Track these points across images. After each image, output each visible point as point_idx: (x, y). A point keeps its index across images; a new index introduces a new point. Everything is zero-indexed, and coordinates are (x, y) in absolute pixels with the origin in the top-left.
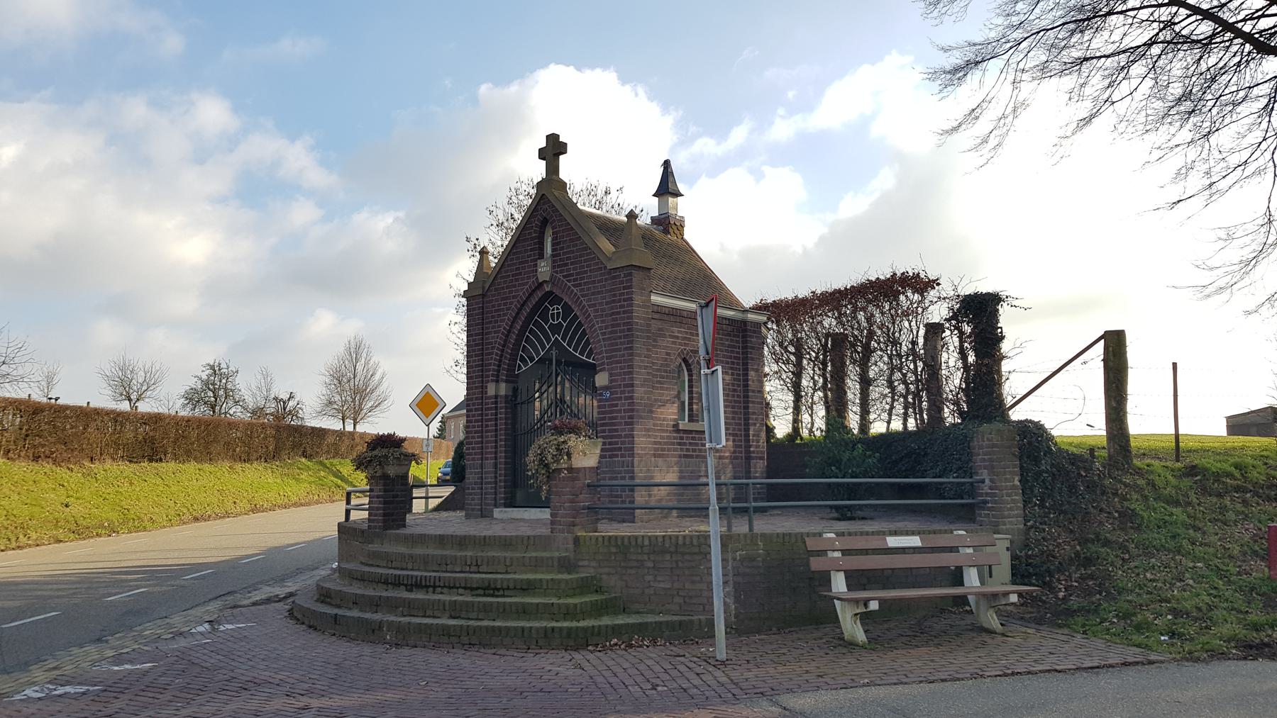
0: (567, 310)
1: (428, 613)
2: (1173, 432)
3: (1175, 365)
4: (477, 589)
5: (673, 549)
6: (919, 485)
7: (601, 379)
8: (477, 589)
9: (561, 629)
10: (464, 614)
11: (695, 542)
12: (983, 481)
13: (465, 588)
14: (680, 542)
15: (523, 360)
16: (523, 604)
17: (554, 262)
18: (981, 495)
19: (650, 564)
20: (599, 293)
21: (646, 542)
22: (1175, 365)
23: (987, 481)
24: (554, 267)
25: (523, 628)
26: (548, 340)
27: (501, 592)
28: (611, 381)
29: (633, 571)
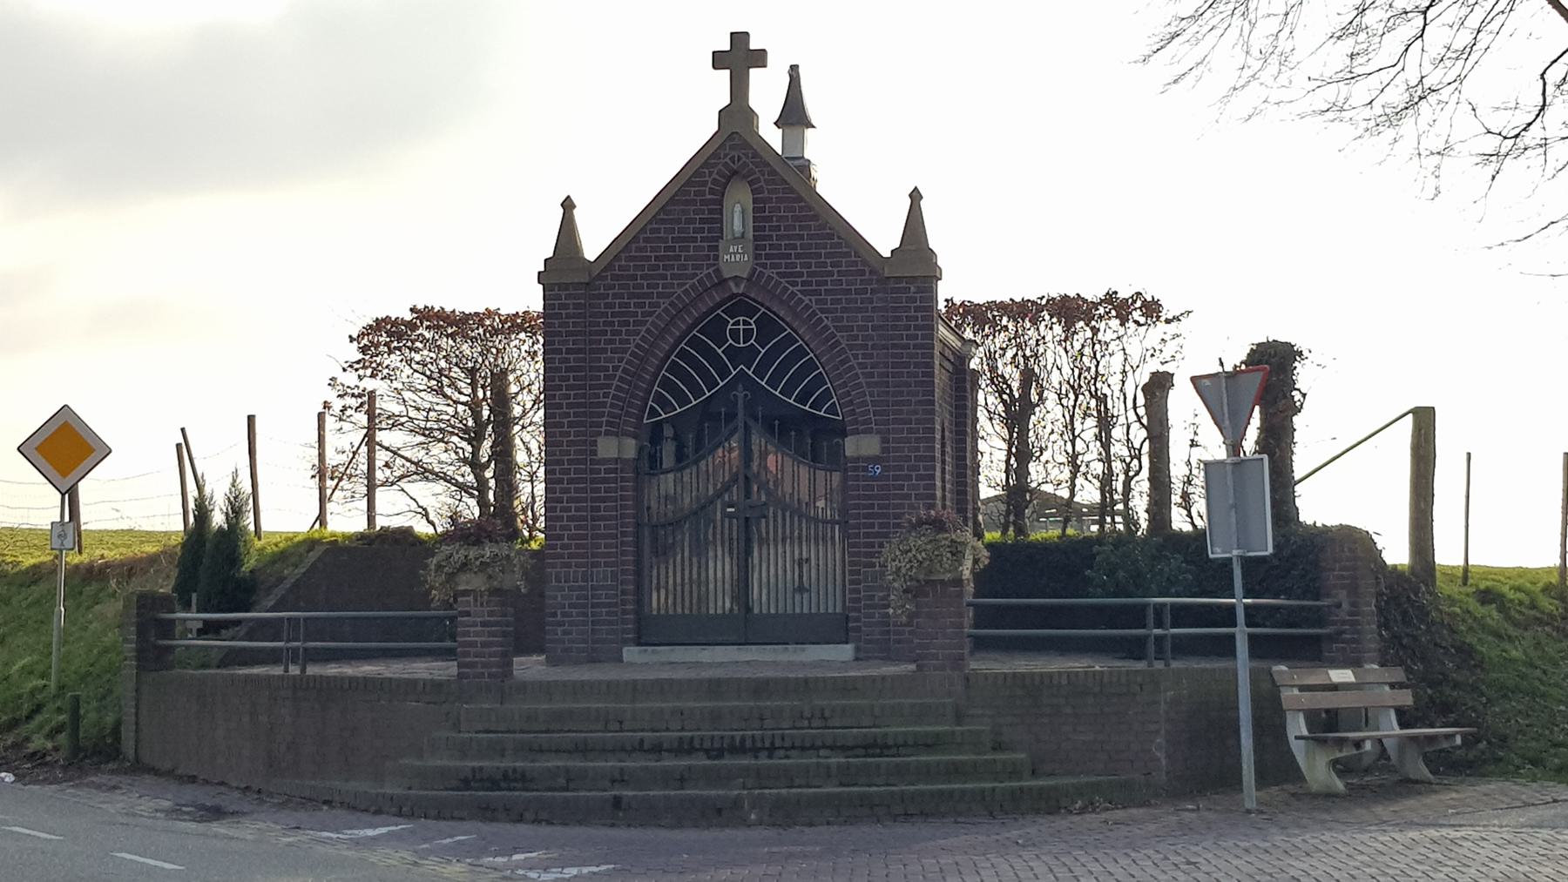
0: (768, 326)
1: (797, 782)
2: (1558, 562)
3: (251, 419)
4: (852, 748)
5: (1097, 689)
6: (1071, 608)
7: (861, 446)
8: (852, 748)
9: (1030, 789)
10: (503, 784)
11: (1123, 680)
12: (1339, 606)
13: (832, 748)
14: (1106, 680)
15: (660, 399)
16: (954, 763)
17: (757, 248)
18: (1334, 623)
19: (1069, 710)
20: (859, 310)
21: (1064, 682)
22: (251, 419)
23: (1345, 606)
24: (757, 257)
25: (983, 791)
26: (724, 373)
27: (894, 751)
28: (884, 450)
29: (1046, 720)
